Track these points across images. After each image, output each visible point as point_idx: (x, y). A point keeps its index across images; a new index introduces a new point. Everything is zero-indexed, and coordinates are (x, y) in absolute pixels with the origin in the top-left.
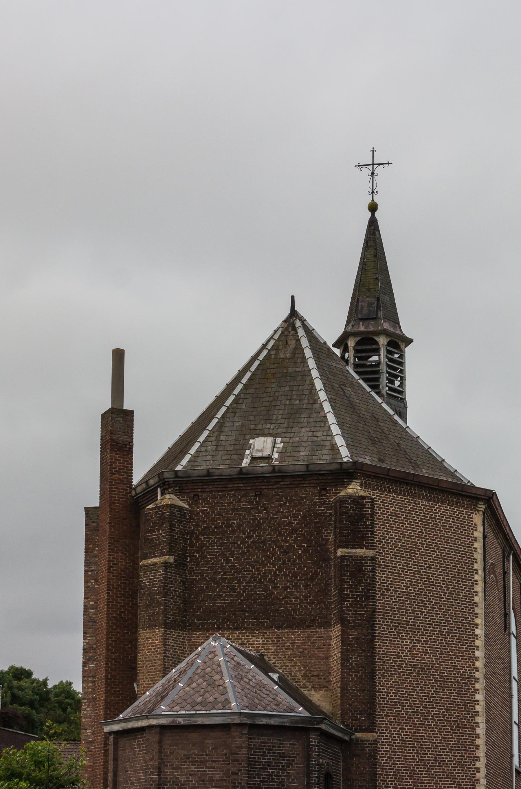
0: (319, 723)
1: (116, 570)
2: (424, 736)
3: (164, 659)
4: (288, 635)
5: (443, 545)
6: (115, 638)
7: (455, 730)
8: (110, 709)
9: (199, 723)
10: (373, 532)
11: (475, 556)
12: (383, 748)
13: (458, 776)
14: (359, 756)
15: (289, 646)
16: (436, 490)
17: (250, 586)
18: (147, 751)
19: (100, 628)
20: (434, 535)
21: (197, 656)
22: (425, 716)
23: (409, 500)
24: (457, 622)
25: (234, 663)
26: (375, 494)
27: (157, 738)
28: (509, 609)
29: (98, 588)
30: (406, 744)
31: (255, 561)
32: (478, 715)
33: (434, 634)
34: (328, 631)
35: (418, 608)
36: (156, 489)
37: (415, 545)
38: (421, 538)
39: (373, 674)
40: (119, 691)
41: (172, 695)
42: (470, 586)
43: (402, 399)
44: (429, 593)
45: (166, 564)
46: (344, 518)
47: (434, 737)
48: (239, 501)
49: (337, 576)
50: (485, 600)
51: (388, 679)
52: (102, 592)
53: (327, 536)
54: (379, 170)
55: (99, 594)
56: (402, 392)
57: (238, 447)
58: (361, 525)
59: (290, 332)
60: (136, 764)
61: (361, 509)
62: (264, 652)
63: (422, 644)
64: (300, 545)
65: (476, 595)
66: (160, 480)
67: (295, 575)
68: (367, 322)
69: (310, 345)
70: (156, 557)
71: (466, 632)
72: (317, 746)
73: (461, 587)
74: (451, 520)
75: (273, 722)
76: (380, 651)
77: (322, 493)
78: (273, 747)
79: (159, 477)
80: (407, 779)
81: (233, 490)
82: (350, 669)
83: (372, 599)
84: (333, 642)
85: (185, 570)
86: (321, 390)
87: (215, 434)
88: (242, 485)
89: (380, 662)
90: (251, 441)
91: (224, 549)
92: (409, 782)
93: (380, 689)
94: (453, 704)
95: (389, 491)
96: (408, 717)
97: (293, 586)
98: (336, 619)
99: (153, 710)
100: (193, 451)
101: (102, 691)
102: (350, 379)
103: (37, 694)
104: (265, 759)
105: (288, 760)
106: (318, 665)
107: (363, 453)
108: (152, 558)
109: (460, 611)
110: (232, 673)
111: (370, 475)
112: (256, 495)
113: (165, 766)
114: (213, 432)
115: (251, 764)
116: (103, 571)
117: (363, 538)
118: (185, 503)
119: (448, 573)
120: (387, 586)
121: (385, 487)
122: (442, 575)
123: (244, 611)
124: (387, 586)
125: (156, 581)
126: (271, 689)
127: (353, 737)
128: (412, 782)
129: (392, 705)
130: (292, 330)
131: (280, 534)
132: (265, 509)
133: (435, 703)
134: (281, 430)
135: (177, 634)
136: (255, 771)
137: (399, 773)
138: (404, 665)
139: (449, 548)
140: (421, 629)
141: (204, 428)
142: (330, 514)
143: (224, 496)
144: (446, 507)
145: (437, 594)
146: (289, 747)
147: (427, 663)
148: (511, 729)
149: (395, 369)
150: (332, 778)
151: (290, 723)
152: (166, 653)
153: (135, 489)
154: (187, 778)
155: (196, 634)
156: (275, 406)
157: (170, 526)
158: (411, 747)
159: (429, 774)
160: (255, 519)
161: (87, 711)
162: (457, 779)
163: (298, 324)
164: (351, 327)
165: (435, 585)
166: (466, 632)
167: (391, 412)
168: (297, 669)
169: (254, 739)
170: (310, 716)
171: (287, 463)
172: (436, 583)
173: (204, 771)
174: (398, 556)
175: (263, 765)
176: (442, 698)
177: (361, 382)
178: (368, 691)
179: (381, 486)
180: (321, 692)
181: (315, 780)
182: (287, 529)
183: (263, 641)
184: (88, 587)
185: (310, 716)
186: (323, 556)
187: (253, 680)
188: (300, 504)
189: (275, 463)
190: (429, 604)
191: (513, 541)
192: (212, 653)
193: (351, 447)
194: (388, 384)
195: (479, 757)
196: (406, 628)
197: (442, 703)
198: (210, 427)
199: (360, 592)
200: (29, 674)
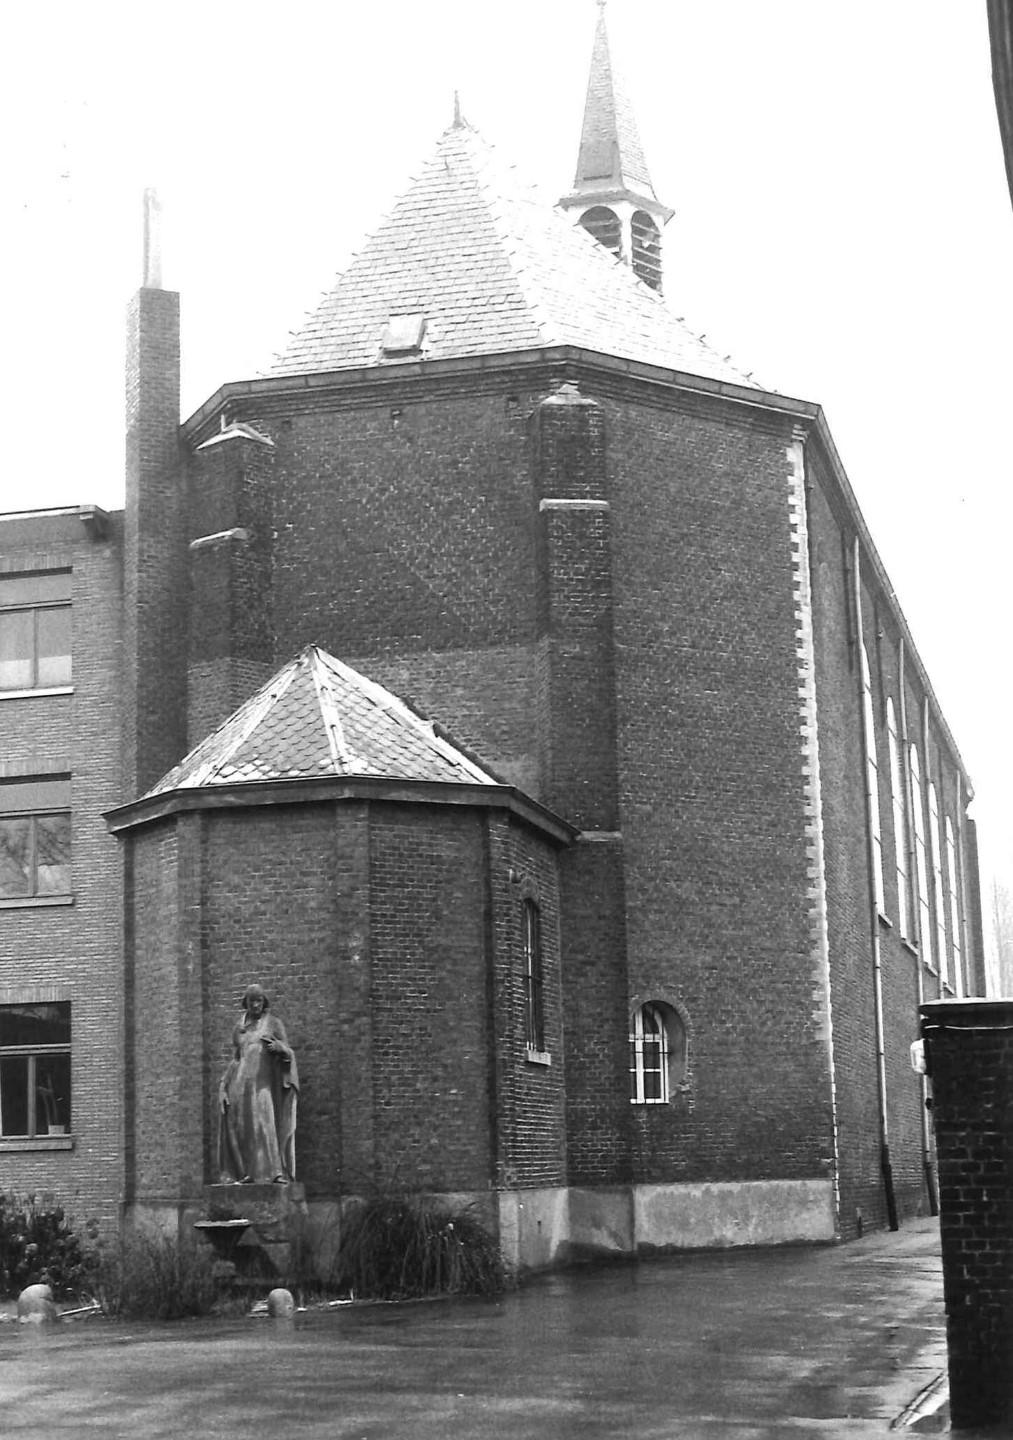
31: (394, 532)
81: (352, 409)
115: (375, 878)
127: (579, 838)
131: (437, 482)
169: (380, 829)
170: (495, 783)
185: (495, 783)
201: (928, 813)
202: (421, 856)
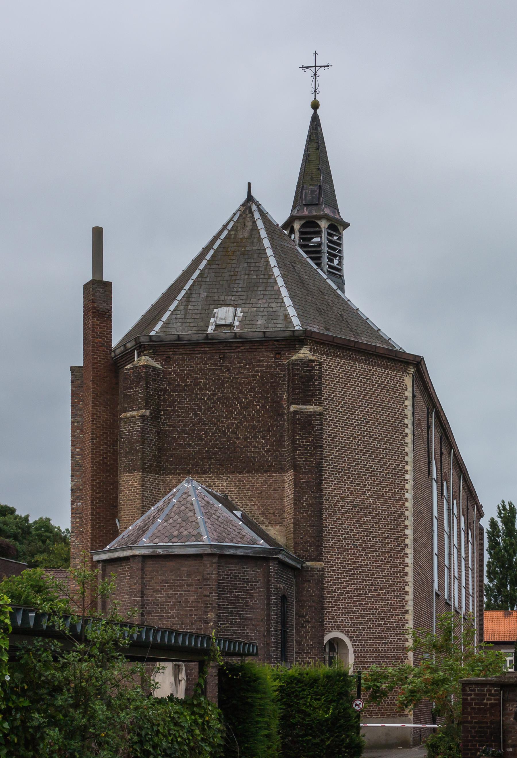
0: (276, 554)
1: (98, 422)
2: (362, 565)
3: (143, 498)
4: (248, 479)
5: (380, 402)
6: (99, 481)
7: (388, 559)
8: (95, 541)
9: (176, 553)
10: (320, 391)
11: (406, 413)
12: (328, 575)
13: (391, 598)
14: (309, 581)
15: (249, 488)
16: (373, 355)
17: (215, 437)
18: (131, 577)
19: (86, 471)
20: (371, 394)
21: (172, 496)
22: (364, 548)
23: (351, 363)
24: (391, 469)
25: (205, 503)
26: (322, 358)
27: (140, 566)
28: (432, 458)
29: (84, 437)
30: (347, 571)
31: (219, 415)
32: (408, 547)
33: (371, 478)
34: (282, 476)
35: (358, 457)
36: (132, 352)
37: (356, 403)
38: (360, 396)
39: (321, 512)
40: (103, 526)
41: (152, 529)
42: (402, 438)
43: (340, 276)
44: (367, 444)
45: (143, 417)
46: (296, 379)
47: (371, 565)
48: (206, 363)
49: (290, 428)
50: (413, 450)
51: (333, 516)
52: (87, 441)
53: (282, 394)
54: (320, 72)
55: (84, 442)
56: (340, 270)
57: (203, 316)
58: (311, 385)
59: (247, 214)
60: (122, 588)
61: (310, 371)
62: (228, 493)
63: (362, 487)
64: (259, 402)
65: (407, 446)
66: (136, 344)
67: (254, 428)
68: (310, 207)
69: (265, 227)
70: (134, 410)
71: (398, 477)
72: (275, 573)
73: (395, 439)
74: (386, 381)
75: (239, 552)
76: (326, 493)
77: (277, 357)
78: (239, 573)
79: (135, 341)
80: (348, 600)
81: (200, 353)
82: (301, 508)
83: (320, 448)
84: (286, 485)
85: (159, 422)
86: (275, 266)
87: (184, 304)
88: (208, 349)
89: (326, 502)
90: (215, 311)
91: (193, 404)
92: (350, 603)
93: (326, 525)
94: (387, 538)
95: (334, 355)
96: (349, 549)
97: (252, 437)
98: (289, 466)
99: (136, 542)
100: (165, 318)
101: (88, 526)
102: (299, 257)
103: (20, 528)
104: (232, 584)
105: (251, 585)
106: (274, 504)
107: (311, 322)
108: (131, 411)
109: (393, 460)
110: (203, 510)
111: (318, 342)
112: (220, 358)
113: (146, 589)
114: (182, 302)
115: (220, 588)
116: (88, 423)
117: (312, 396)
118: (158, 364)
119: (383, 427)
120: (332, 438)
121: (330, 352)
122: (378, 429)
123: (211, 458)
124: (332, 438)
125: (135, 431)
126: (236, 525)
127: (304, 565)
128: (352, 603)
129: (337, 538)
130: (249, 213)
131: (241, 392)
132: (228, 370)
133: (371, 537)
134: (241, 301)
135: (153, 477)
136: (224, 594)
137: (342, 595)
138: (346, 505)
139: (384, 406)
140: (360, 475)
141: (174, 299)
142: (284, 375)
143: (192, 358)
144: (382, 370)
145: (374, 445)
146: (252, 574)
147: (365, 504)
148: (432, 559)
149: (335, 249)
150: (287, 600)
151: (253, 553)
152: (143, 494)
153: (114, 351)
154: (166, 599)
155: (169, 477)
156: (235, 280)
157: (146, 384)
158: (352, 574)
159: (366, 597)
160: (219, 378)
161: (75, 543)
162: (390, 600)
163: (254, 208)
164: (296, 211)
165: (372, 437)
166: (398, 477)
167: (335, 287)
168: (256, 508)
169: (223, 566)
171: (246, 330)
172: (373, 435)
173: (181, 594)
174: (341, 412)
175: (231, 589)
176: (378, 533)
177: (309, 260)
178: (316, 526)
179: (327, 351)
180: (277, 527)
181: (274, 602)
182: (247, 388)
183: (227, 484)
184: (75, 436)
186: (278, 411)
187: (221, 517)
188: (258, 366)
189: (236, 330)
190: (367, 453)
191: (436, 400)
192: (185, 493)
193: (302, 317)
194: (329, 263)
195: (407, 582)
196: (348, 473)
197: (377, 537)
198: (179, 298)
199: (310, 442)
200: (12, 511)
201: (460, 531)
202: (239, 578)
